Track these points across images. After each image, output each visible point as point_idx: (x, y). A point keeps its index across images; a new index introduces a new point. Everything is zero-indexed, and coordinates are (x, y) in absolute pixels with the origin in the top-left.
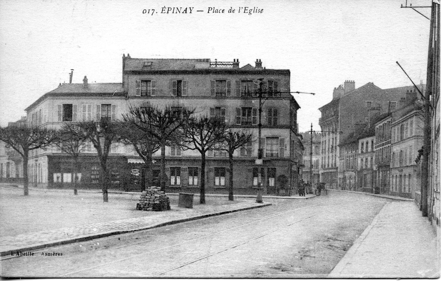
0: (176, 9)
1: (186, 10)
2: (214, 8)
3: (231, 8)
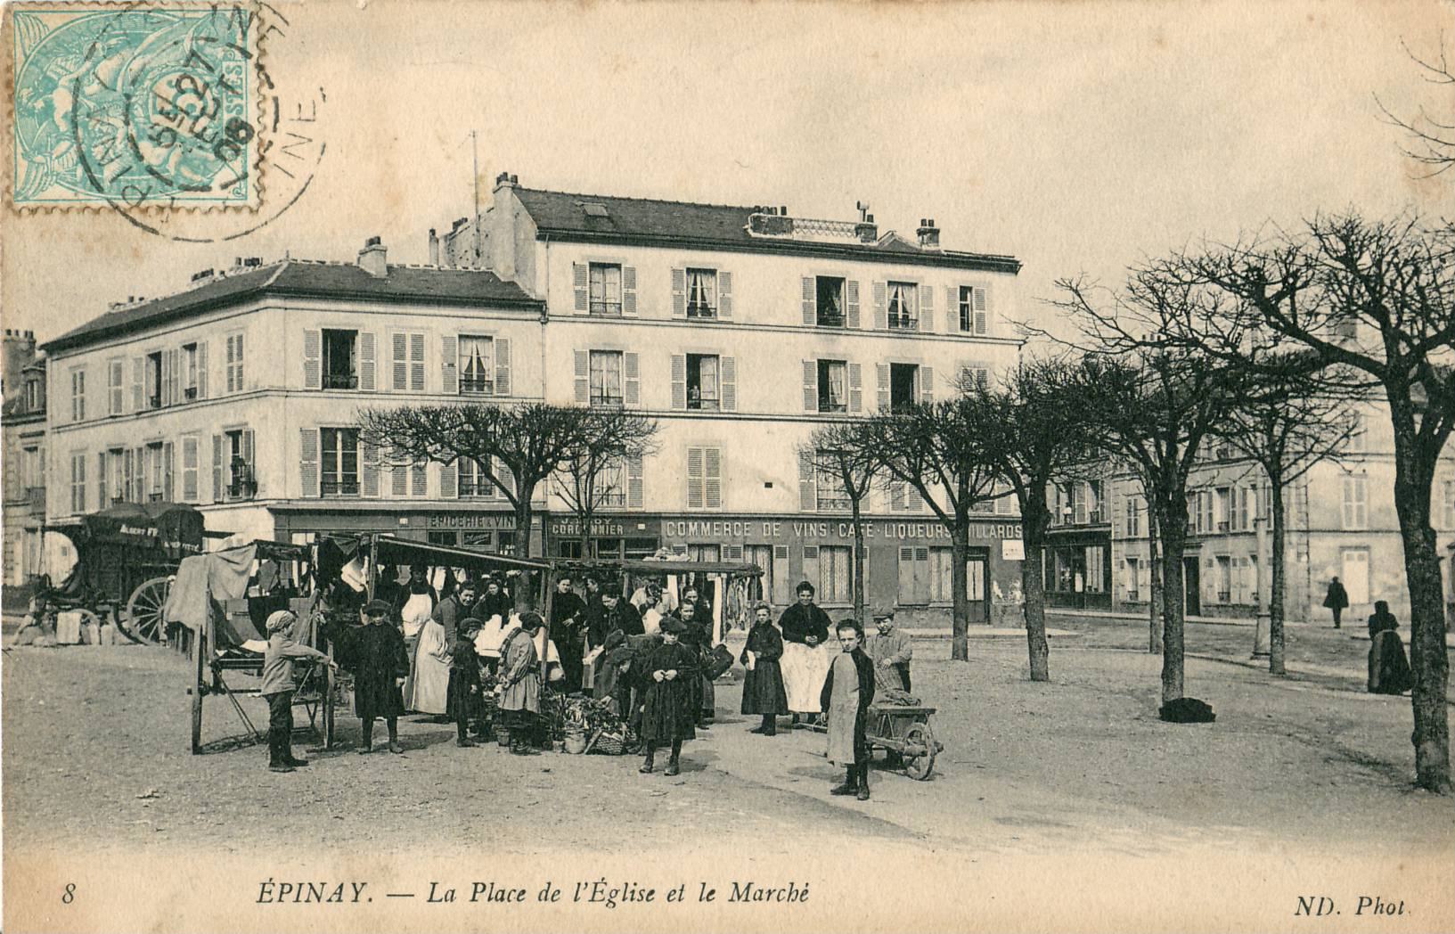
2: (492, 884)
3: (549, 884)
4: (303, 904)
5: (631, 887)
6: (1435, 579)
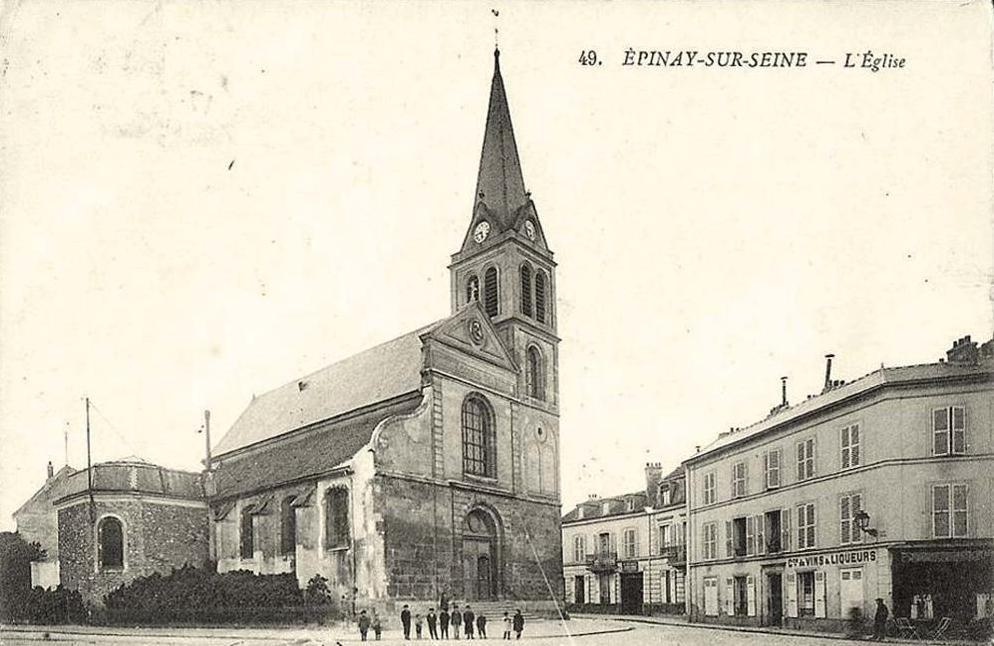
0: (781, 57)
1: (679, 60)
3: (853, 66)
4: (654, 67)
5: (889, 58)
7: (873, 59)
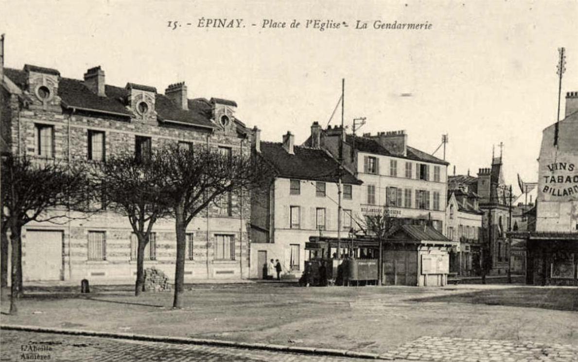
0: (218, 22)
5: (330, 22)
6: (556, 242)
7: (320, 23)
